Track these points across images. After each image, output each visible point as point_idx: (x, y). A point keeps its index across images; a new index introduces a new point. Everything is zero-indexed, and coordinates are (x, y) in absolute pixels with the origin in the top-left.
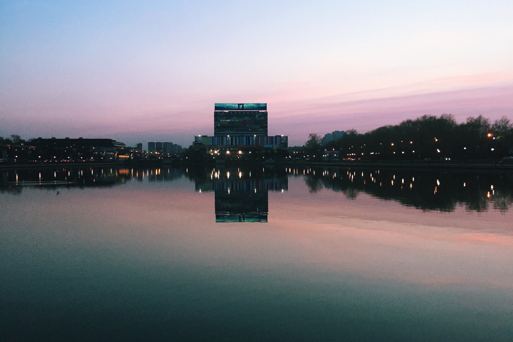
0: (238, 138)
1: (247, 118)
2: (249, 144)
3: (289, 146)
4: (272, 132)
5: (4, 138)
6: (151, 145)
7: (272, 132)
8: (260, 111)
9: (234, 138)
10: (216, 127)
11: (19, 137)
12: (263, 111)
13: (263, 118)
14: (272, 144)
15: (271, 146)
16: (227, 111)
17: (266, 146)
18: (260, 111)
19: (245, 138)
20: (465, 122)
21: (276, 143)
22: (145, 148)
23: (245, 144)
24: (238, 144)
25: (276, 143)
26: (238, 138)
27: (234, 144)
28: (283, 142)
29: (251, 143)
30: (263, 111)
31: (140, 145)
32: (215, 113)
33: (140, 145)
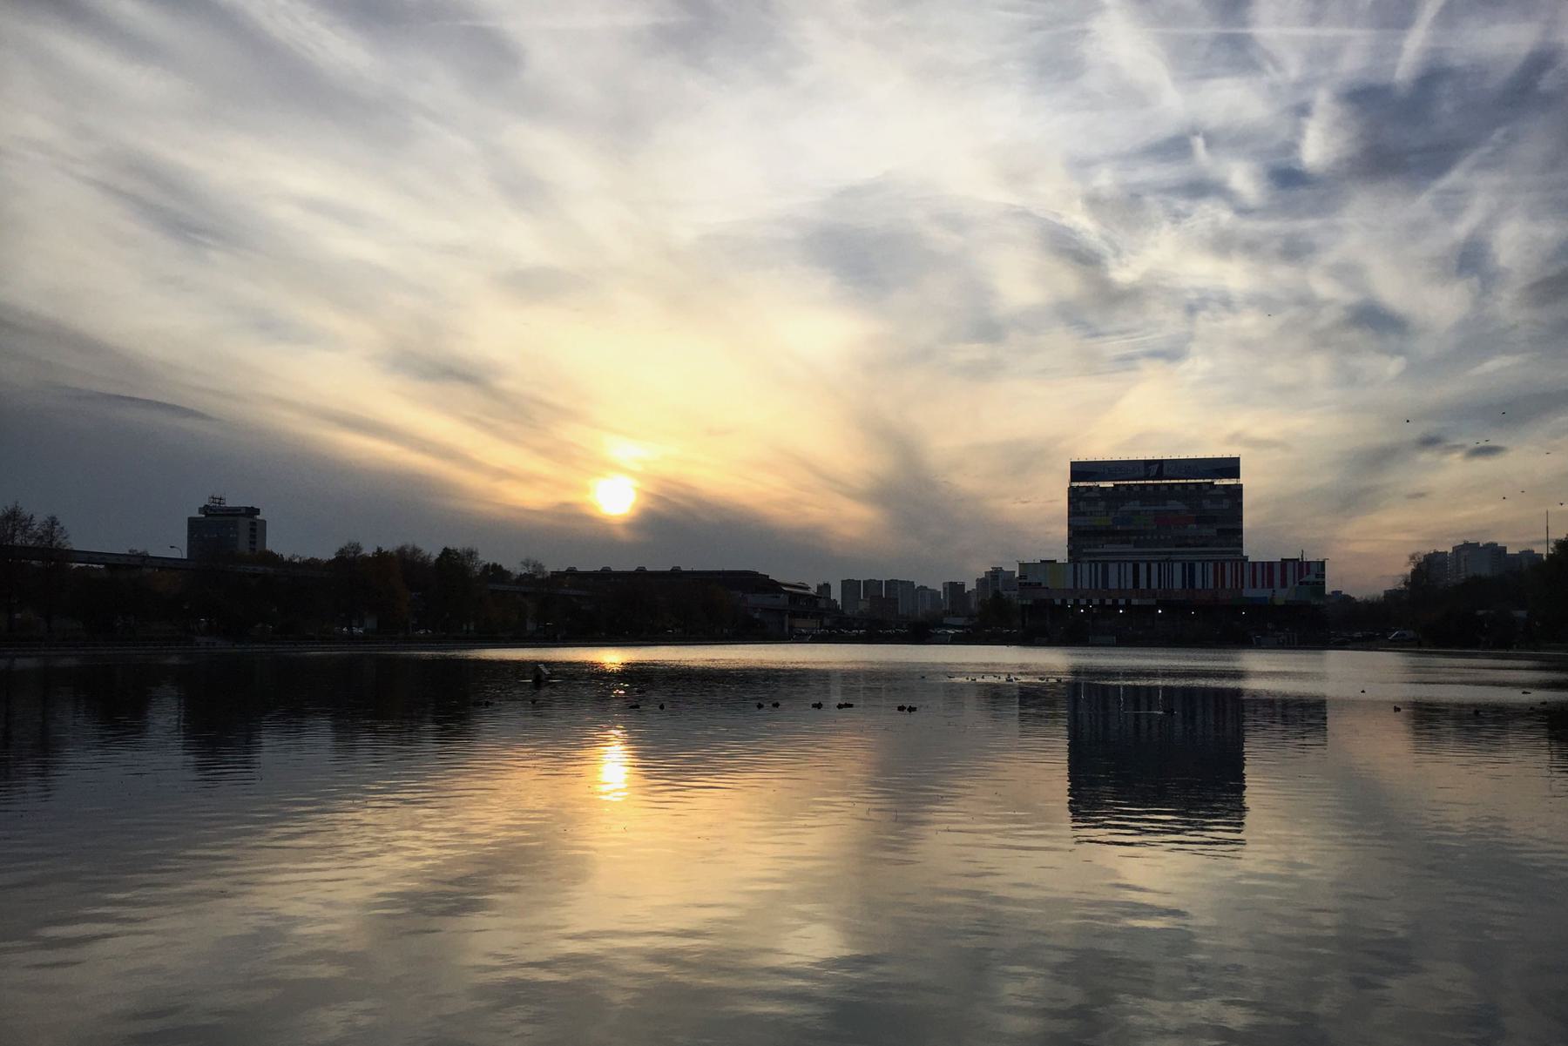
0: (1154, 567)
1: (1174, 505)
2: (1192, 585)
3: (1328, 590)
4: (1256, 546)
5: (1542, 550)
6: (849, 586)
7: (1256, 546)
8: (1217, 482)
9: (1143, 567)
10: (1072, 538)
11: (541, 566)
12: (1226, 482)
13: (1226, 504)
14: (1271, 584)
15: (1267, 593)
16: (1110, 484)
17: (1249, 592)
18: (1217, 482)
19: (1178, 567)
20: (286, 557)
21: (1284, 584)
22: (836, 594)
23: (1178, 584)
24: (1154, 584)
25: (1284, 584)
26: (1154, 567)
27: (1143, 585)
28: (1312, 578)
29: (1199, 585)
30: (1226, 482)
31: (826, 588)
32: (1071, 490)
33: (826, 588)
